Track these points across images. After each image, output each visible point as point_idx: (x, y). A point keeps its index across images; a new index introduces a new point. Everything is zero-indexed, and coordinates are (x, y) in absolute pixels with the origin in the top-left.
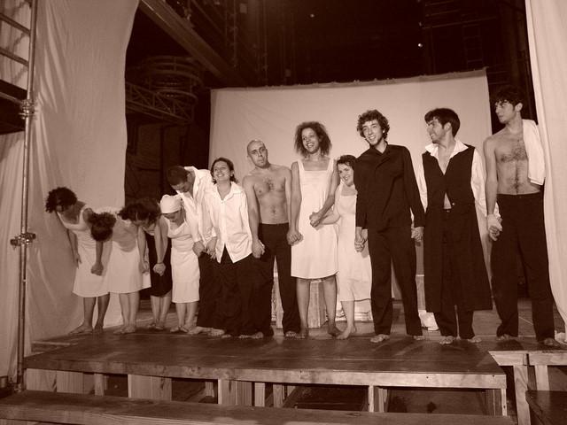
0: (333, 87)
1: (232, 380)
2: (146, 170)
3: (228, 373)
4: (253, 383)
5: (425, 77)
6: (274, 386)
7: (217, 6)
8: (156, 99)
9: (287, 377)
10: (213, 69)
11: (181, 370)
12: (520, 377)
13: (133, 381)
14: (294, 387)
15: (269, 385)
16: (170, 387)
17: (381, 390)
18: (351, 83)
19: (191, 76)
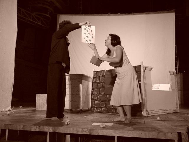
0: (109, 15)
3: (52, 129)
5: (148, 13)
6: (93, 87)
7: (116, 41)
10: (58, 5)
12: (184, 137)
18: (117, 15)
19: (48, 8)
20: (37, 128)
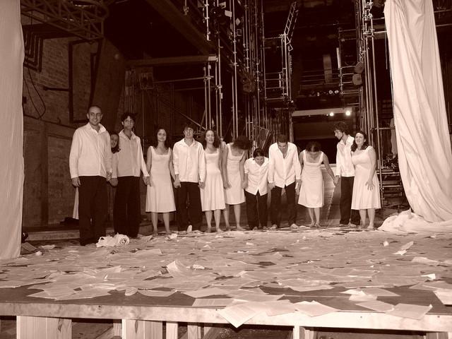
1: (138, 320)
2: (51, 89)
3: (133, 312)
4: (164, 323)
8: (63, 8)
9: (201, 316)
11: (79, 310)
13: (22, 322)
14: (210, 328)
15: (183, 325)
16: (70, 329)
17: (307, 332)
20: (94, 310)
